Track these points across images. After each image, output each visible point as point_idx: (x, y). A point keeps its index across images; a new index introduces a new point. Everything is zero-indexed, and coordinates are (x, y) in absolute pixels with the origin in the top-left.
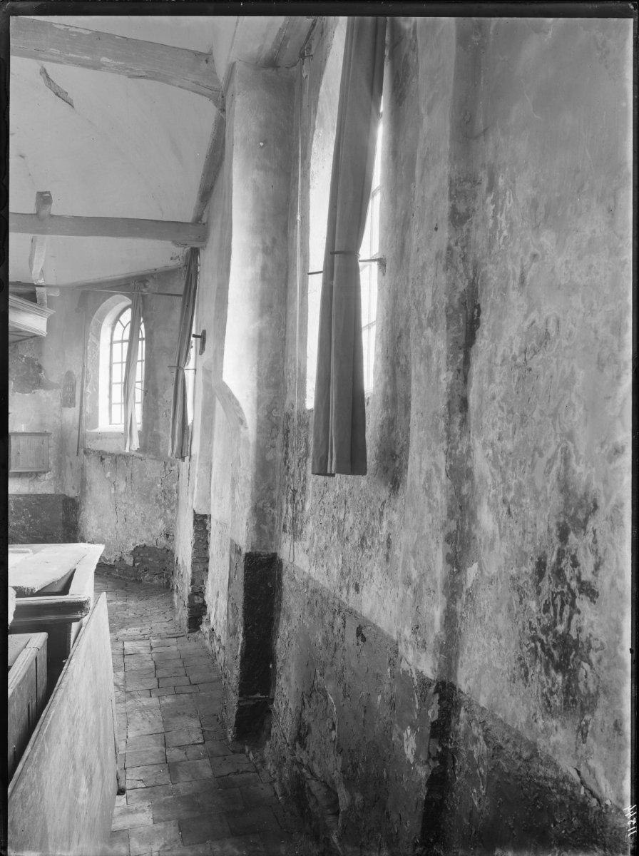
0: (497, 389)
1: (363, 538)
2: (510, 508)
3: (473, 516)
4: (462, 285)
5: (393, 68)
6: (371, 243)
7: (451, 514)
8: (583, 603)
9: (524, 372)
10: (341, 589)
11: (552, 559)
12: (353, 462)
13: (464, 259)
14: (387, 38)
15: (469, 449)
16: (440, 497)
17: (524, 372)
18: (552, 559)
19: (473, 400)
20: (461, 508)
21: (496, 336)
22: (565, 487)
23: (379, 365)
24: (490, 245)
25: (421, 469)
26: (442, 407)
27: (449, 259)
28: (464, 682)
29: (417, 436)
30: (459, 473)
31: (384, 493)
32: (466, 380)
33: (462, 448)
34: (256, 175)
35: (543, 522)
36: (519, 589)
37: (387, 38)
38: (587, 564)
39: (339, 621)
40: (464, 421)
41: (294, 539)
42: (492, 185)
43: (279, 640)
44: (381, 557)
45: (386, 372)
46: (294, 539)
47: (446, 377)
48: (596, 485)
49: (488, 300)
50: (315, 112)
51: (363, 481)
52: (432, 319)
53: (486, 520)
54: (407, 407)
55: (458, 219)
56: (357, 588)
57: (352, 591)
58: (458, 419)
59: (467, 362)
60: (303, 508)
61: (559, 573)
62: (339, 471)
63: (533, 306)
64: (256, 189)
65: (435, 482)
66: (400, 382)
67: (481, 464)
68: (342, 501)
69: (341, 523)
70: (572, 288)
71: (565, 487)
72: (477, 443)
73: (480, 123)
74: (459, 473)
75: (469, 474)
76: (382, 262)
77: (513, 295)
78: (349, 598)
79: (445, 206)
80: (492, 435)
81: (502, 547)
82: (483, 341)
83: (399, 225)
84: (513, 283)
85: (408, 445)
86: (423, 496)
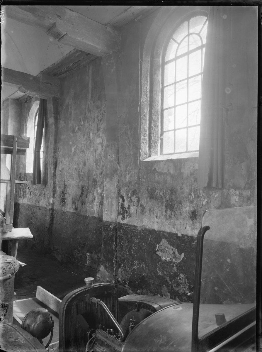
0: (59, 174)
1: (40, 195)
2: (60, 187)
3: (56, 189)
4: (55, 161)
5: (46, 123)
6: (42, 149)
7: (53, 188)
8: (65, 195)
9: (61, 172)
10: (35, 204)
11: (63, 191)
12: (39, 182)
13: (55, 158)
14: (45, 119)
15: (56, 181)
16: (52, 186)
17: (61, 172)
18: (63, 191)
19: (56, 175)
20: (55, 188)
21: (59, 168)
22: (64, 184)
23: (43, 167)
24: (58, 156)
25: (196, 117)
26: (52, 175)
27: (53, 157)
28: (55, 208)
29: (49, 178)
30: (54, 183)
31: (44, 187)
32: (55, 172)
33: (55, 180)
34: (14, 123)
35: (62, 188)
36: (60, 195)
37: (45, 119)
38: (66, 191)
39: (35, 209)
40: (55, 177)
41: (23, 198)
42: (58, 150)
43: (19, 219)
44: (43, 196)
45: (44, 169)
46: (23, 198)
47: (53, 172)
48: (67, 184)
49: (58, 163)
50: (28, 115)
51: (40, 185)
52: (51, 164)
53: (57, 189)
54: (48, 175)
55: (55, 153)
56: (39, 202)
57: (38, 203)
58: (54, 177)
59: (55, 170)
60: (26, 192)
61: (64, 193)
62: (37, 184)
63: (62, 165)
64: (14, 126)
65: (51, 184)
66: (47, 171)
67: (57, 182)
68: (36, 189)
69: (35, 193)
70: (65, 165)
71: (64, 184)
72: (57, 180)
73: (57, 142)
74: (54, 183)
75: (56, 183)
76: (43, 152)
77: (60, 163)
78: (37, 204)
79: (53, 151)
80: (58, 179)
81: (59, 191)
82: (57, 168)
83: (47, 147)
84: (61, 162)
85: (48, 180)
86: (50, 186)
